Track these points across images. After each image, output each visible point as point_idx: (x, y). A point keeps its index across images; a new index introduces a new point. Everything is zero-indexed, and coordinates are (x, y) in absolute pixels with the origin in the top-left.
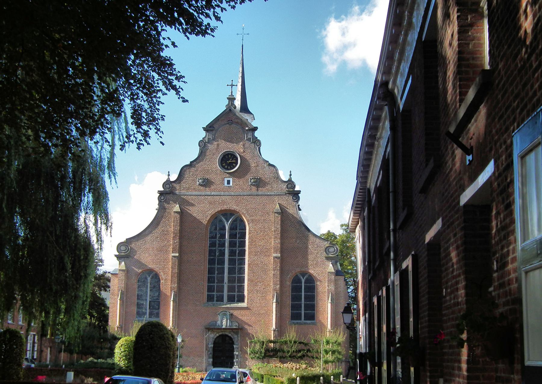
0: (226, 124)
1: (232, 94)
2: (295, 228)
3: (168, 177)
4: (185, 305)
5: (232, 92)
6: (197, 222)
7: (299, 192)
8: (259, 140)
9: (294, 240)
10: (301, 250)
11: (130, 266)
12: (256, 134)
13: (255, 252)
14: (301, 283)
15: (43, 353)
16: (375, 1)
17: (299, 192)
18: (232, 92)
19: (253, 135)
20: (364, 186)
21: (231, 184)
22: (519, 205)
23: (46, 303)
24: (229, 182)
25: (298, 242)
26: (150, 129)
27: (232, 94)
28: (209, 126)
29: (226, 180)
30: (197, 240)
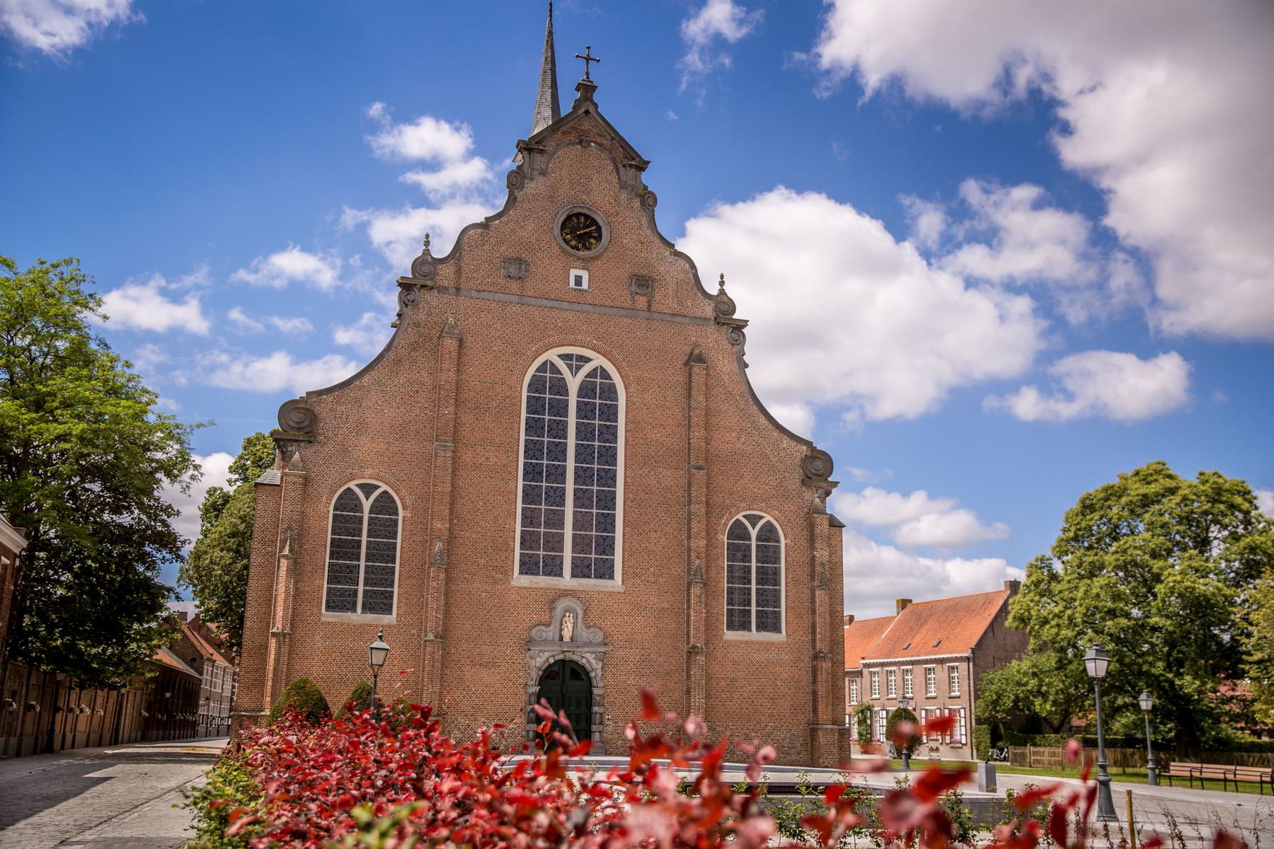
0: (574, 144)
1: (588, 78)
2: (737, 406)
3: (424, 247)
4: (465, 578)
5: (587, 73)
6: (499, 368)
7: (744, 323)
8: (651, 193)
9: (734, 434)
10: (750, 460)
11: (314, 466)
12: (646, 178)
13: (642, 456)
14: (750, 539)
15: (1083, 773)
16: (831, 6)
17: (744, 323)
18: (587, 73)
19: (637, 178)
20: (81, 737)
21: (585, 285)
22: (42, 743)
23: (99, 676)
24: (578, 280)
25: (743, 440)
26: (75, 826)
27: (588, 78)
28: (536, 140)
29: (574, 273)
30: (498, 412)
